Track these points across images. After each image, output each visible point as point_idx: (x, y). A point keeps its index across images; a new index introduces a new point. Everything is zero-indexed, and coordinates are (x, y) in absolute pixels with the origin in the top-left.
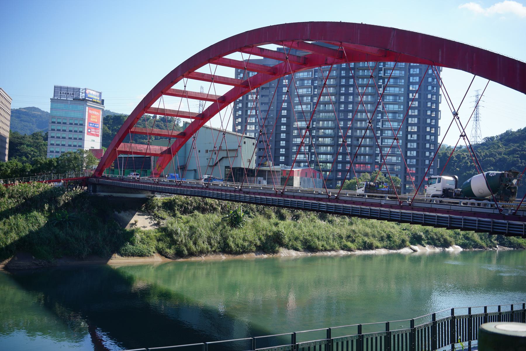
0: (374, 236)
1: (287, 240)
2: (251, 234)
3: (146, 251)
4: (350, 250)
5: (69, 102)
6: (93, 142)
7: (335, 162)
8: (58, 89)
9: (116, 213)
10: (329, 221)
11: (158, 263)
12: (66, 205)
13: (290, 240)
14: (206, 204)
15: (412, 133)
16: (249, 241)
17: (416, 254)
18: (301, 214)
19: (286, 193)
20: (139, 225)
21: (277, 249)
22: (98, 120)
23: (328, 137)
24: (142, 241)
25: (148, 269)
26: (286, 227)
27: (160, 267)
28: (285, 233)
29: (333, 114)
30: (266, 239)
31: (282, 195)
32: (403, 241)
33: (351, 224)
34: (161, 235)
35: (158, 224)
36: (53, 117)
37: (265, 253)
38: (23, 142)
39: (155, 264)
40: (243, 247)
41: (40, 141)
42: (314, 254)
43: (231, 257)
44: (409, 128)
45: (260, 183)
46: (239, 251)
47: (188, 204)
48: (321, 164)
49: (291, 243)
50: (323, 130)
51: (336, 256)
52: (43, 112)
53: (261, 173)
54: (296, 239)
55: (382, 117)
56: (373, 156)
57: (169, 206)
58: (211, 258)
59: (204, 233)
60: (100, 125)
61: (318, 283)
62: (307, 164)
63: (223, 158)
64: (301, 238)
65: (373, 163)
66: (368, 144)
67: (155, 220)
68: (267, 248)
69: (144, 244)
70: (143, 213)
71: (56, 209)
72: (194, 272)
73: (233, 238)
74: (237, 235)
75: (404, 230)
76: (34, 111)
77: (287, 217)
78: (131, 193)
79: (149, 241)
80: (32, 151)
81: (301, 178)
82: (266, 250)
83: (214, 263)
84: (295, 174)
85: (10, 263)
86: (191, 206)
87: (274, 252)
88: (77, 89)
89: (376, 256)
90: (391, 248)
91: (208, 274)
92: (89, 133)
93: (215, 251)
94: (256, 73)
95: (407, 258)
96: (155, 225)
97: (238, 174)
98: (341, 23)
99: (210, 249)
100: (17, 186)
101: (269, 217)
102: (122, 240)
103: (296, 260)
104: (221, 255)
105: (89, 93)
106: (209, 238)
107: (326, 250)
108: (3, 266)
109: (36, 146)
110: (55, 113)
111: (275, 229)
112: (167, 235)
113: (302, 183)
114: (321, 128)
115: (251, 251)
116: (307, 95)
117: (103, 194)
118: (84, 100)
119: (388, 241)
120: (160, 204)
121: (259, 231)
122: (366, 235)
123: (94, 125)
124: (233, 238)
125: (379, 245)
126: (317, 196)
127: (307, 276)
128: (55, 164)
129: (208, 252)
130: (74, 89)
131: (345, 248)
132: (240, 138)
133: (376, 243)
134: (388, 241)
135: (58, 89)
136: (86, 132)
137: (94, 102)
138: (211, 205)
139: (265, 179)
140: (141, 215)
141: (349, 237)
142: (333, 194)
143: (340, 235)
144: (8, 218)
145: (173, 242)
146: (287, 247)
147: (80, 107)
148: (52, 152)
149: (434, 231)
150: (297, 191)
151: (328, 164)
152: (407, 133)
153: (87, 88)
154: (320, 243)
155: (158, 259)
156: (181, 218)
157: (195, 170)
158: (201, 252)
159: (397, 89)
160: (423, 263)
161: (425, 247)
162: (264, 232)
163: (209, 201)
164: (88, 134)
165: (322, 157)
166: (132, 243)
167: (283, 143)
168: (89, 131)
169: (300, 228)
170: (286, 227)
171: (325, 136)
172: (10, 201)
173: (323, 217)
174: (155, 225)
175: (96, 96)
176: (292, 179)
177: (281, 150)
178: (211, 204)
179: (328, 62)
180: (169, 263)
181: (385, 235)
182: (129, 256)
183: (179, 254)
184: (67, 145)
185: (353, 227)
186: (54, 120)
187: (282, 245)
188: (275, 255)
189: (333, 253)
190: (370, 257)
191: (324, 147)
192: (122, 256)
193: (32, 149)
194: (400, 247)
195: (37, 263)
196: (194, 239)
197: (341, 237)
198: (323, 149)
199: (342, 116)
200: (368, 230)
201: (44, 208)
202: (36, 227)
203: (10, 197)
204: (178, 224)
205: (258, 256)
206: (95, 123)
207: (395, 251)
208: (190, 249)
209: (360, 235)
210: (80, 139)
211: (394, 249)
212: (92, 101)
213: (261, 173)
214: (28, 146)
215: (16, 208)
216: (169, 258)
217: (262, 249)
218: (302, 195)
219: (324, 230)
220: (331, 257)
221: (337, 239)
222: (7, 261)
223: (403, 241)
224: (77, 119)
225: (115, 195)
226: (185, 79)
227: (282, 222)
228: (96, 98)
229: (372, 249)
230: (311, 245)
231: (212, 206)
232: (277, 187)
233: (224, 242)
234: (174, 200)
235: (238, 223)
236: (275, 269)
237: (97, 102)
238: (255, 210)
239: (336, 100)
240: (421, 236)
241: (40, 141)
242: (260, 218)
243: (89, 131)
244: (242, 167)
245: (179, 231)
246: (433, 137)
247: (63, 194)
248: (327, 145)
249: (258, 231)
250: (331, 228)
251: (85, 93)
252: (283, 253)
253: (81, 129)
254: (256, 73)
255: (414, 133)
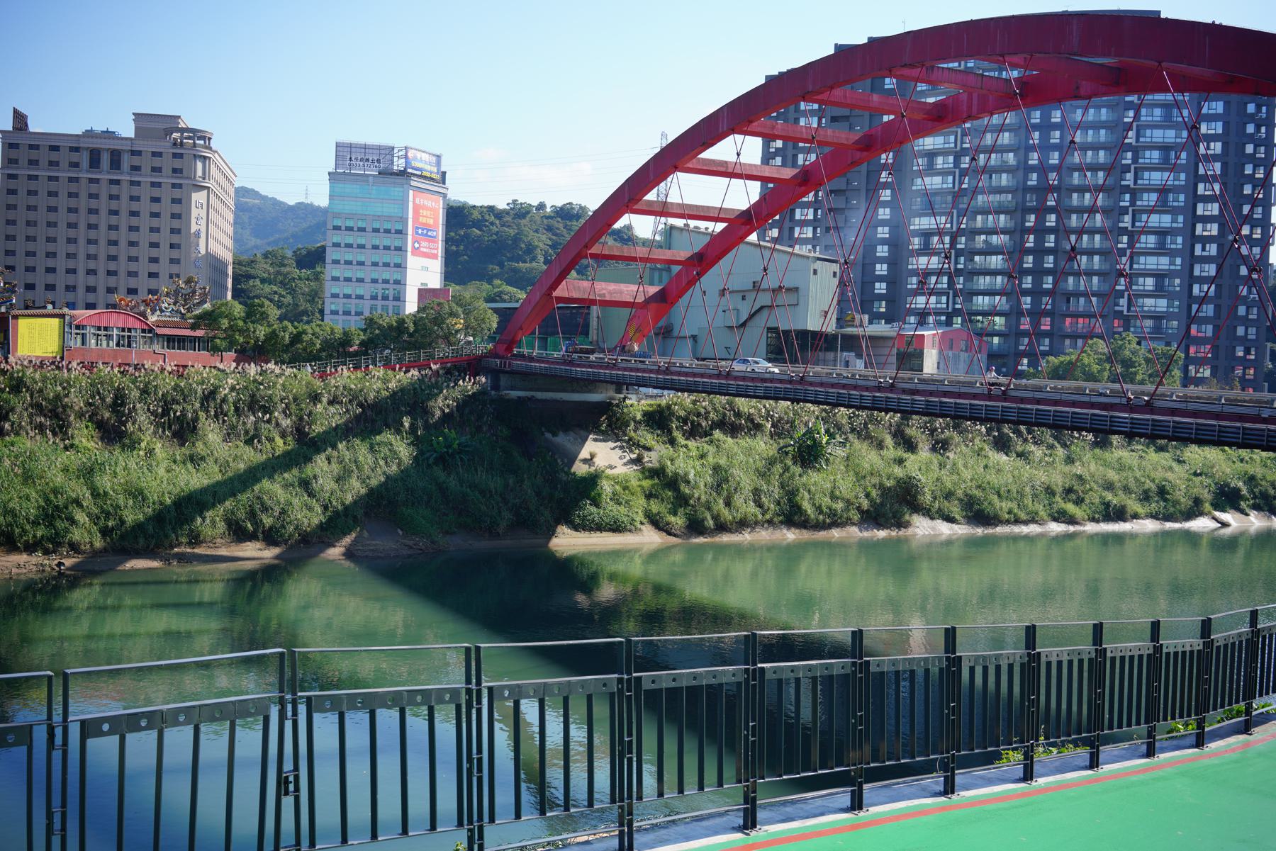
0: (1127, 489)
1: (927, 498)
2: (846, 486)
3: (625, 519)
4: (1072, 521)
5: (371, 179)
6: (424, 272)
7: (1014, 314)
8: (345, 151)
9: (548, 435)
10: (1019, 455)
11: (653, 547)
12: (446, 418)
13: (935, 498)
14: (738, 415)
15: (1205, 240)
16: (843, 499)
17: (1226, 532)
18: (952, 438)
19: (1013, 393)
20: (600, 462)
21: (907, 517)
22: (436, 221)
23: (996, 253)
24: (616, 499)
25: (632, 558)
26: (921, 465)
27: (655, 555)
28: (924, 480)
29: (1010, 196)
30: (882, 496)
31: (1004, 396)
32: (1198, 501)
33: (1070, 460)
34: (653, 486)
35: (638, 461)
36: (337, 215)
37: (880, 526)
38: (252, 271)
39: (645, 549)
40: (833, 513)
41: (288, 269)
42: (990, 531)
43: (806, 535)
44: (1199, 227)
45: (847, 364)
46: (824, 521)
47: (699, 415)
48: (980, 318)
49: (937, 505)
50: (983, 237)
51: (1041, 535)
52: (264, 198)
53: (851, 343)
54: (949, 495)
55: (1133, 202)
56: (1109, 296)
57: (658, 420)
58: (764, 535)
59: (745, 479)
60: (440, 233)
61: (990, 596)
62: (943, 318)
63: (762, 308)
64: (960, 493)
65: (1109, 314)
66: (1096, 267)
67: (631, 451)
68: (884, 515)
69: (620, 504)
70: (604, 436)
71: (427, 427)
72: (728, 569)
73: (809, 491)
74: (816, 485)
75: (1195, 474)
76: (244, 196)
77: (921, 445)
78: (573, 391)
79: (630, 497)
80: (276, 293)
81: (941, 353)
82: (882, 520)
83: (770, 548)
84: (927, 343)
85: (355, 542)
86: (706, 419)
87: (901, 524)
88: (386, 148)
89: (1133, 536)
90: (1168, 518)
91: (754, 574)
92: (416, 252)
93: (770, 522)
94: (892, 117)
95: (1205, 541)
96: (632, 462)
97: (786, 345)
98: (1213, 27)
99: (760, 517)
100: (345, 377)
101: (880, 445)
102: (574, 498)
103: (949, 542)
104: (785, 531)
105: (415, 158)
106: (756, 492)
107: (1017, 521)
108: (343, 549)
109: (281, 282)
110: (347, 207)
111: (898, 471)
112: (666, 483)
113: (942, 365)
114: (980, 232)
115: (848, 522)
116: (944, 153)
117: (515, 394)
118: (403, 173)
119: (1162, 501)
120: (639, 417)
121: (864, 477)
122: (1109, 486)
123: (425, 233)
124: (809, 491)
125: (1140, 510)
126: (1094, 399)
127: (962, 582)
128: (412, 329)
129: (756, 523)
130: (380, 148)
131: (1060, 517)
132: (786, 258)
133: (1133, 505)
134: (1162, 501)
135: (345, 151)
136: (409, 249)
137: (425, 177)
138: (750, 419)
139: (859, 356)
140: (600, 441)
141: (1069, 491)
142: (1138, 395)
143: (1048, 488)
144: (334, 447)
145: (681, 501)
146: (928, 513)
147: (396, 191)
148: (335, 296)
149: (1269, 478)
150: (931, 381)
151: (997, 319)
152: (1193, 239)
153: (409, 145)
154: (1004, 504)
155: (650, 538)
156: (686, 446)
157: (694, 338)
158: (742, 524)
159: (1171, 134)
160: (1241, 552)
161: (1247, 515)
162: (876, 480)
163: (742, 404)
164: (413, 254)
165: (982, 302)
166: (596, 503)
167: (881, 269)
168: (417, 245)
169: (955, 470)
170: (921, 465)
171: (989, 251)
172: (332, 410)
173: (1002, 445)
174: (632, 462)
175: (430, 164)
176: (920, 355)
177: (877, 285)
178: (750, 414)
179: (1082, 92)
180: (674, 546)
181: (1153, 487)
182: (591, 530)
183: (695, 527)
184: (368, 280)
185: (1078, 469)
186: (338, 223)
187: (917, 509)
188: (902, 532)
189: (1033, 529)
190: (1119, 538)
191: (988, 278)
192: (576, 530)
193: (275, 288)
194: (1190, 515)
195: (411, 543)
196: (725, 493)
197: (1050, 491)
198: (983, 282)
199: (1031, 200)
200: (1112, 475)
201: (402, 425)
202: (395, 468)
203: (331, 403)
204: (688, 459)
205: (866, 534)
206: (429, 228)
207: (1177, 526)
208: (718, 515)
209: (1095, 487)
210: (398, 266)
211: (1176, 521)
212: (420, 176)
213: (851, 343)
214: (263, 281)
215: (346, 424)
216: (675, 535)
217: (873, 517)
218: (1057, 397)
219: (1009, 475)
220: (1027, 538)
221: (1042, 496)
222: (347, 540)
223: (1198, 501)
224: (389, 218)
225: (540, 395)
226: (739, 137)
227: (913, 457)
228: (428, 167)
229: (1125, 521)
230: (983, 511)
231: (752, 421)
232: (887, 374)
233: (790, 500)
234: (669, 407)
235: (816, 459)
236: (902, 562)
237: (431, 179)
238: (847, 428)
239: (1019, 162)
240: (1239, 490)
241: (288, 269)
242: (859, 446)
243: (417, 245)
244: (810, 328)
245: (691, 476)
246: (1256, 250)
247: (437, 395)
248: (993, 273)
249: (860, 477)
250: (1027, 471)
251: (406, 157)
252: (922, 528)
253: (397, 243)
254: (892, 117)
255: (1210, 239)
